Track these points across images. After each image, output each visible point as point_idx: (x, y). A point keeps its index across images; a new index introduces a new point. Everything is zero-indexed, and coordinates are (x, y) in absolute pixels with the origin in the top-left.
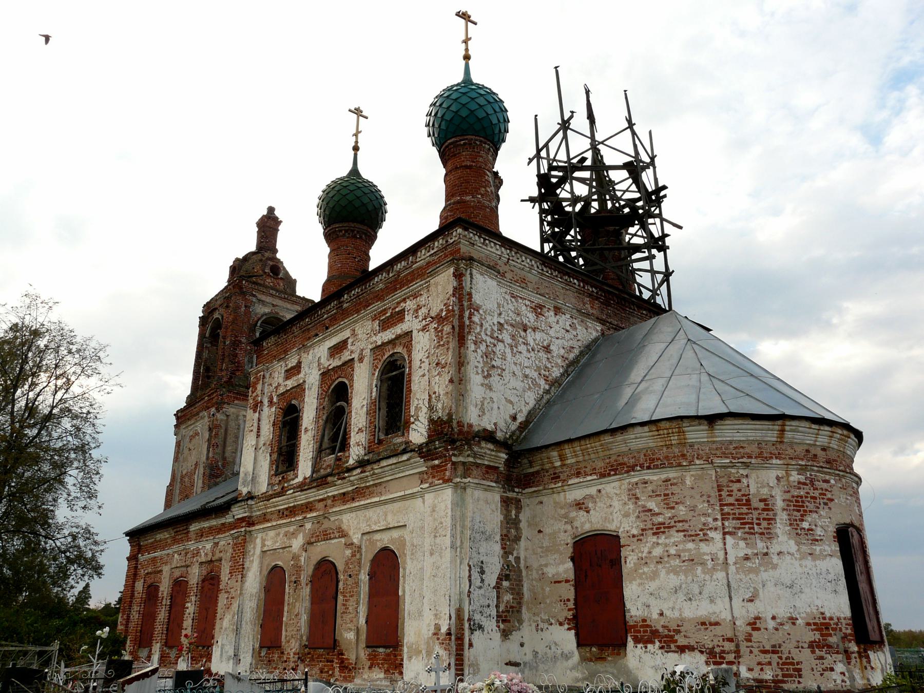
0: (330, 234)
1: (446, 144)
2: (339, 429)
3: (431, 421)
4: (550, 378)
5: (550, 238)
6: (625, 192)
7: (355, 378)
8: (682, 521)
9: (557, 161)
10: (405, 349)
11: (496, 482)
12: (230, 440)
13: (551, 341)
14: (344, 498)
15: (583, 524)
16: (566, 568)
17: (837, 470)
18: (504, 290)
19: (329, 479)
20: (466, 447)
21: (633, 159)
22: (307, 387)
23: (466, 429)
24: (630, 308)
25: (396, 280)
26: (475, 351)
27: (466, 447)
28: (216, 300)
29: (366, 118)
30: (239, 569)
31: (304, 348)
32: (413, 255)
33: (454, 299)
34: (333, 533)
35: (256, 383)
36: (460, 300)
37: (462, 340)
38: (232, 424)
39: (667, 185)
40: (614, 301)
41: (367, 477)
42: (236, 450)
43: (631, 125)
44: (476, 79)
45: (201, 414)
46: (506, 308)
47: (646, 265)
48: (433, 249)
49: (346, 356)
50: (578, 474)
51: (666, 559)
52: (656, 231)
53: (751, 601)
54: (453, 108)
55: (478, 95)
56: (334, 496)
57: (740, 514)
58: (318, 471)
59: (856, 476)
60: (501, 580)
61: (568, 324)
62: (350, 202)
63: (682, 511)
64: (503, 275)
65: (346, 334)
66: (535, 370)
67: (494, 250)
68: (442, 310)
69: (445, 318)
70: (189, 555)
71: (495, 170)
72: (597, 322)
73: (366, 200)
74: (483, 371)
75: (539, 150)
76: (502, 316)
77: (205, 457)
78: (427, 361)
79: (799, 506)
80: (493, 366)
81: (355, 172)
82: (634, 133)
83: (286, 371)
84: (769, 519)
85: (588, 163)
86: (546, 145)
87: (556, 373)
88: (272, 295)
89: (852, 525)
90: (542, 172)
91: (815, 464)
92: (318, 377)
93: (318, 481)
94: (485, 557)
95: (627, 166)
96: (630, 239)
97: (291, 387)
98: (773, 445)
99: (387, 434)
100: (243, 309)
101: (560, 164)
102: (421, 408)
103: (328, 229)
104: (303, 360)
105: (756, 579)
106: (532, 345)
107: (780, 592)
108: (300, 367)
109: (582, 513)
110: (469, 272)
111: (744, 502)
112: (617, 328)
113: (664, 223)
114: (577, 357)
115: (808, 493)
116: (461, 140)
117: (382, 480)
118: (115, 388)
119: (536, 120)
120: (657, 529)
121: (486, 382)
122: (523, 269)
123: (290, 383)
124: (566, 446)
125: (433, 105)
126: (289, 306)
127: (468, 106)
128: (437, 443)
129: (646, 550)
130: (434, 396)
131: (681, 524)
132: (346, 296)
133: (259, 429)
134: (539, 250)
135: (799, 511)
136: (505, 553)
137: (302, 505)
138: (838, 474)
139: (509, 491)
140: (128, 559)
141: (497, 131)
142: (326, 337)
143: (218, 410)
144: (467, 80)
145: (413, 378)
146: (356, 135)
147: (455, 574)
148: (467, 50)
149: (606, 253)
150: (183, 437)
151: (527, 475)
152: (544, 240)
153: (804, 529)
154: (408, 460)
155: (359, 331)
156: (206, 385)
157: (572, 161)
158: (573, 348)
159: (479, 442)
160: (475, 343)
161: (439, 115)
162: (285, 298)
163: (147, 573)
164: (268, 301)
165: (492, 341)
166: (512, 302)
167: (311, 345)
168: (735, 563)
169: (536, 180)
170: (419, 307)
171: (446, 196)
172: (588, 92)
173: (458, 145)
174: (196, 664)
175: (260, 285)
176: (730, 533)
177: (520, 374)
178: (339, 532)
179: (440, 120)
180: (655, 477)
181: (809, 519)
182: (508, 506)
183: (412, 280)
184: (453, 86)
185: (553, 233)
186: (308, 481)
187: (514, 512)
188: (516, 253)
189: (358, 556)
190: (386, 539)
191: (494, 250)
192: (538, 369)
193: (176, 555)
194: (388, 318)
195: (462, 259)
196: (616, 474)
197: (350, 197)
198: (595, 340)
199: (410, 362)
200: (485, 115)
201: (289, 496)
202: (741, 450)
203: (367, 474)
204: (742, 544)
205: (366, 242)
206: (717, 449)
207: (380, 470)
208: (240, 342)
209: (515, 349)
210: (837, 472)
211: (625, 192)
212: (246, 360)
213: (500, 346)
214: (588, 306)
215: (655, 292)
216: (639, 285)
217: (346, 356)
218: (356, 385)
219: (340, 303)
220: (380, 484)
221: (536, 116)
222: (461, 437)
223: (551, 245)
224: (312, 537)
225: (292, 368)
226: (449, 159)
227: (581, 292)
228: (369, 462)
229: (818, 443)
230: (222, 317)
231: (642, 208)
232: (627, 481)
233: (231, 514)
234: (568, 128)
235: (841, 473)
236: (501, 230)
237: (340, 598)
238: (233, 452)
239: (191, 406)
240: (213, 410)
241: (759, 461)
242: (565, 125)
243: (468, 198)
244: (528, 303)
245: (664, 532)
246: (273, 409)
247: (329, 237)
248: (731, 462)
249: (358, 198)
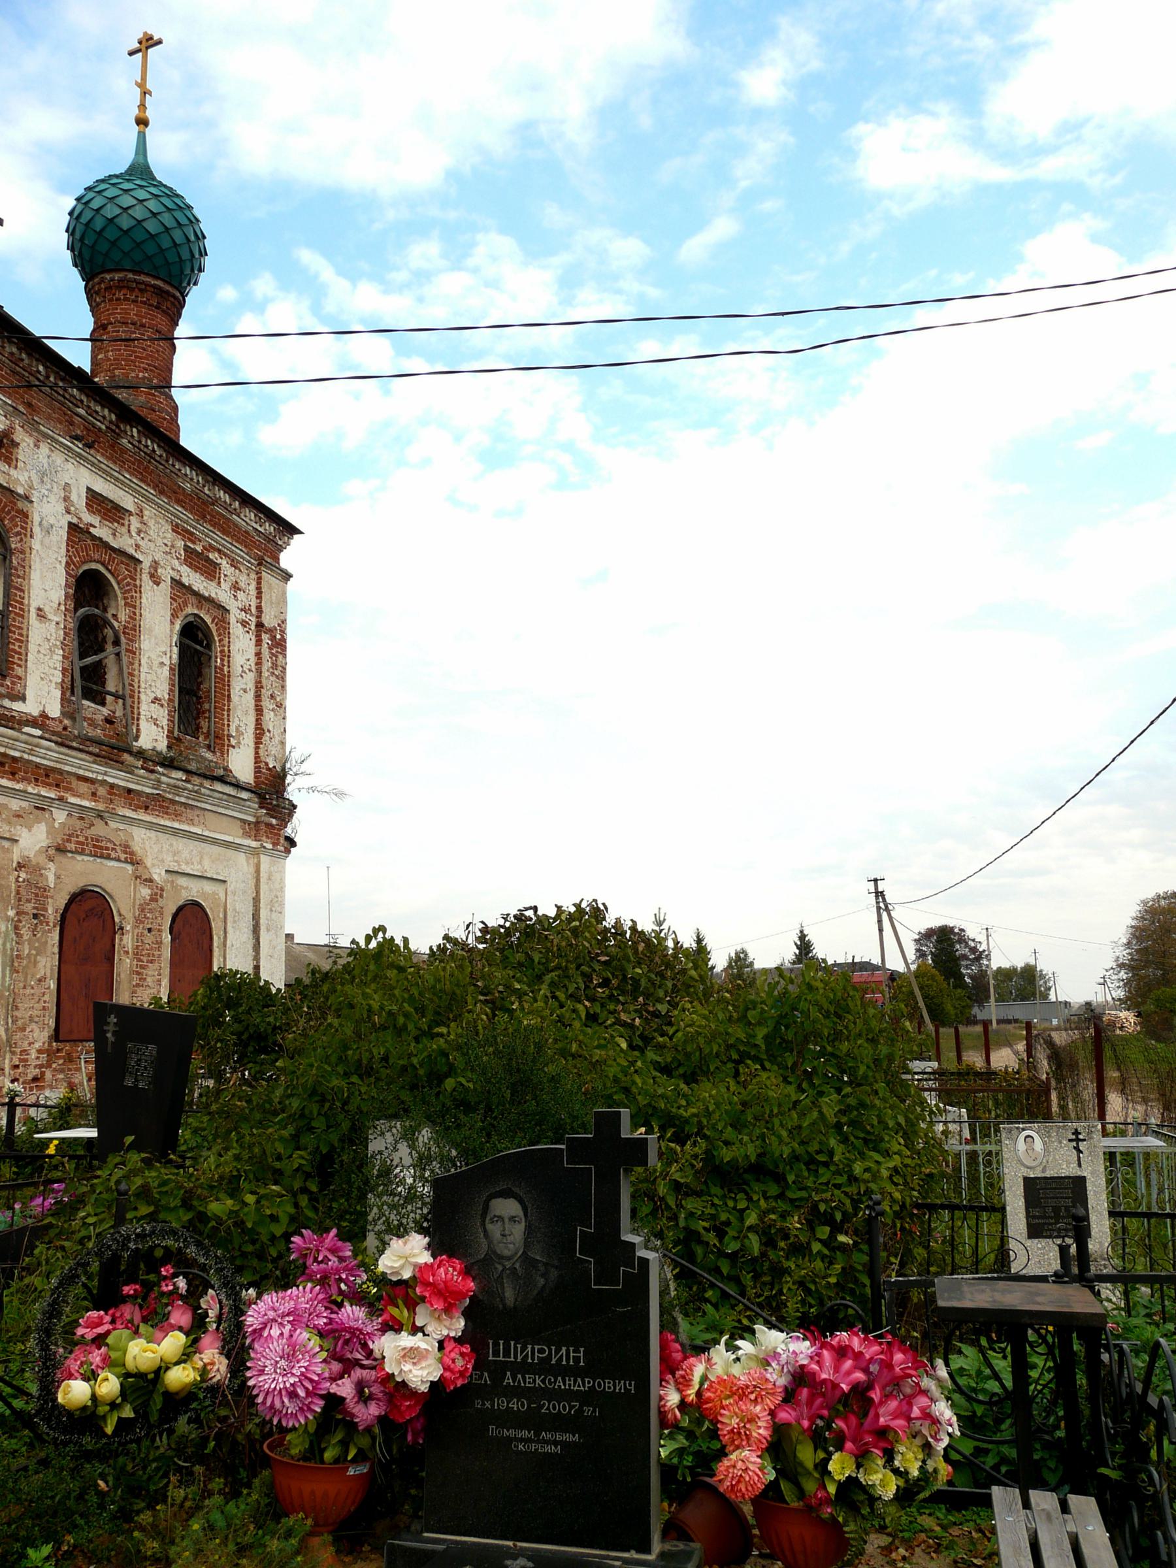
39: (5, 223)
41: (185, 789)
56: (112, 786)
117: (199, 804)
137: (38, 766)
178: (126, 853)
190: (195, 890)
201: (24, 737)
203: (189, 786)
220: (192, 807)
224: (69, 841)
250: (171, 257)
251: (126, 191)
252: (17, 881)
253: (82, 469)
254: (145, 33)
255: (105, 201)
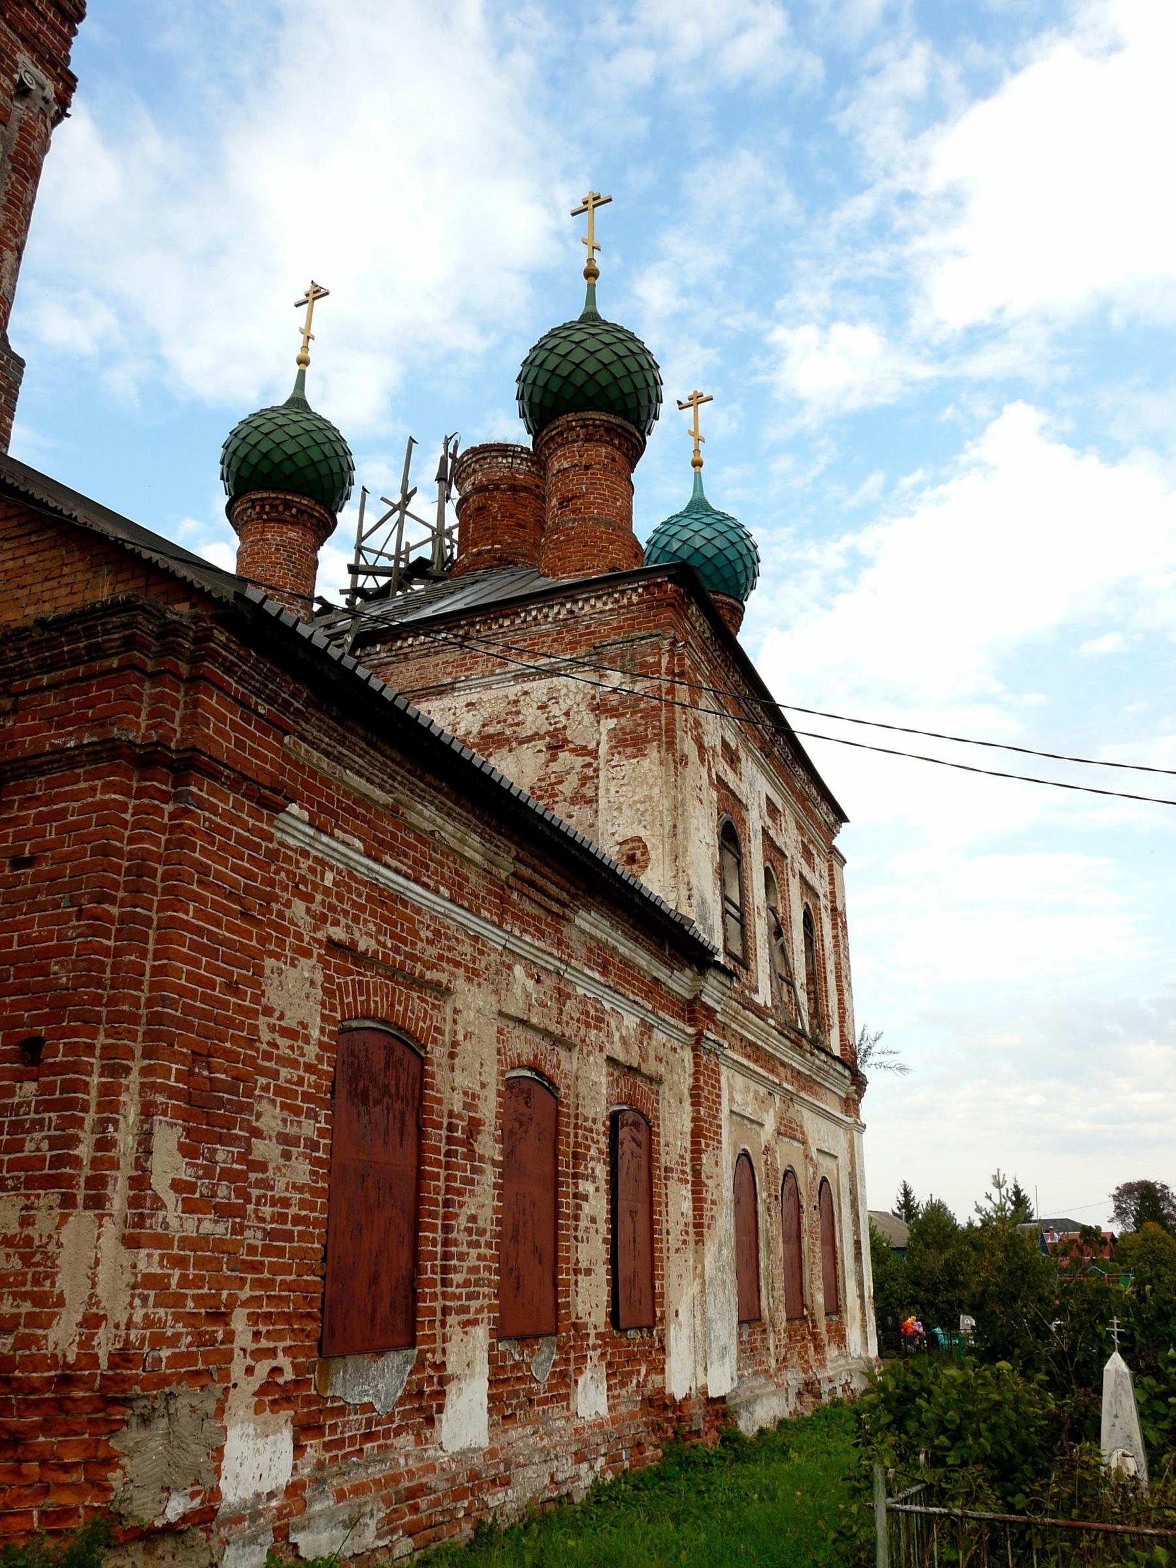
174: (623, 1384)
250: (727, 573)
251: (708, 525)
252: (766, 1164)
254: (695, 392)
255: (260, 437)
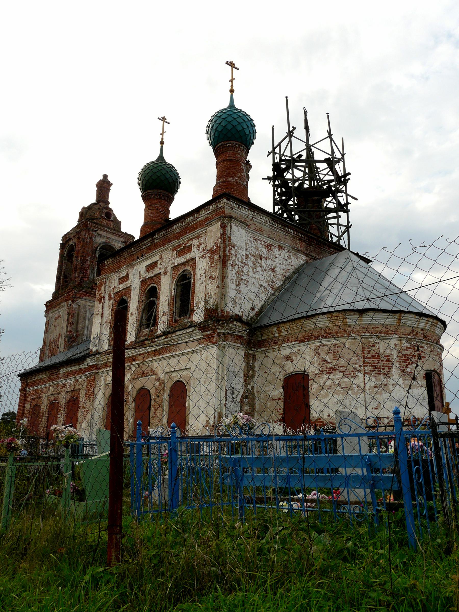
0: (146, 196)
1: (218, 145)
2: (152, 313)
3: (206, 309)
4: (275, 287)
5: (279, 203)
6: (325, 175)
7: (162, 284)
8: (342, 367)
9: (285, 156)
10: (192, 268)
11: (242, 344)
12: (80, 321)
13: (276, 265)
14: (155, 353)
15: (289, 368)
16: (278, 392)
17: (428, 341)
18: (250, 235)
19: (146, 342)
20: (225, 324)
21: (330, 157)
22: (132, 289)
23: (225, 314)
24: (324, 247)
25: (187, 228)
26: (232, 270)
27: (225, 324)
28: (71, 233)
29: (169, 123)
30: (91, 394)
31: (131, 265)
32: (197, 214)
33: (221, 240)
34: (148, 373)
35: (100, 286)
36: (224, 241)
37: (224, 264)
38: (82, 310)
40: (314, 243)
42: (85, 326)
43: (330, 135)
44: (238, 105)
45: (62, 304)
46: (250, 245)
47: (335, 221)
48: (209, 210)
49: (156, 271)
50: (288, 341)
51: (333, 387)
52: (342, 200)
53: (377, 409)
54: (223, 124)
55: (238, 117)
57: (373, 363)
58: (139, 338)
59: (440, 345)
60: (244, 398)
61: (286, 255)
62: (159, 177)
63: (342, 362)
64: (249, 227)
65: (157, 258)
66: (266, 282)
67: (244, 212)
68: (213, 246)
69: (215, 251)
70: (59, 388)
71: (247, 160)
72: (303, 255)
73: (168, 176)
74: (236, 282)
75: (274, 148)
76: (248, 250)
77: (65, 331)
78: (204, 275)
79: (406, 360)
80: (242, 279)
81: (161, 158)
82: (332, 140)
83: (119, 279)
84: (389, 367)
85: (304, 158)
86: (279, 145)
87: (279, 283)
88: (106, 231)
89: (435, 371)
90: (276, 161)
91: (416, 338)
92: (139, 283)
93: (139, 343)
94: (235, 385)
95: (326, 161)
96: (327, 205)
97: (122, 288)
98: (394, 327)
99: (180, 317)
100: (88, 239)
101: (287, 158)
102: (200, 302)
103: (145, 193)
104: (130, 273)
105: (380, 397)
106: (265, 267)
107: (392, 405)
108: (128, 277)
109: (289, 362)
110: (229, 225)
111: (376, 357)
112: (315, 259)
113: (348, 197)
114: (291, 275)
115: (411, 353)
116: (227, 144)
118: (6, 287)
119: (273, 129)
120: (329, 371)
121: (238, 288)
122: (261, 223)
123: (122, 286)
124: (282, 325)
125: (211, 121)
126: (116, 238)
127: (232, 123)
128: (209, 322)
129: (323, 382)
130: (208, 295)
131: (342, 368)
132: (156, 236)
133: (102, 313)
134: (271, 210)
135: (405, 362)
136: (246, 384)
138: (429, 344)
139: (249, 350)
140: (20, 390)
141: (248, 139)
142: (144, 259)
143: (73, 302)
144: (232, 106)
145: (196, 285)
146: (162, 134)
147: (218, 394)
148: (232, 86)
149: (312, 213)
150: (51, 318)
151: (259, 342)
152: (275, 204)
153: (408, 372)
154: (193, 331)
155: (164, 257)
156: (65, 286)
157: (294, 157)
158: (289, 270)
159: (233, 321)
160: (232, 266)
161: (214, 128)
162: (114, 233)
163: (33, 399)
164: (104, 234)
165: (242, 265)
166: (254, 243)
167: (135, 264)
168: (369, 389)
169: (272, 167)
170: (200, 244)
171: (217, 177)
172: (305, 112)
173: (225, 147)
175: (99, 224)
176: (367, 373)
177: (257, 284)
179: (215, 131)
180: (328, 342)
181: (411, 367)
182: (248, 358)
183: (196, 228)
184: (223, 110)
185: (281, 200)
186: (133, 343)
187: (251, 362)
188: (257, 214)
189: (163, 385)
191: (244, 212)
192: (268, 281)
193: (51, 388)
194: (182, 250)
195: (226, 217)
196: (308, 341)
197: (158, 174)
198: (302, 266)
199: (194, 276)
200: (242, 129)
202: (377, 329)
204: (374, 379)
205: (168, 202)
206: (364, 328)
207: (176, 337)
208: (87, 260)
209: (255, 270)
210: (429, 343)
211: (325, 175)
212: (90, 271)
213: (246, 268)
214: (299, 245)
215: (339, 238)
216: (331, 234)
217: (156, 271)
218: (162, 288)
219: (153, 239)
221: (273, 126)
222: (222, 319)
223: (279, 207)
225: (123, 277)
226: (219, 155)
227: (294, 237)
228: (169, 333)
229: (419, 327)
230: (75, 244)
231: (334, 186)
232: (314, 344)
233: (86, 363)
234: (292, 136)
235: (431, 343)
236: (250, 196)
237: (152, 409)
238: (83, 328)
239: (56, 299)
240: (70, 302)
241: (386, 335)
242: (290, 134)
243: (230, 179)
244: (263, 243)
245: (332, 372)
246: (112, 301)
247: (145, 198)
248: (370, 335)
249: (163, 174)
253: (169, 286)
